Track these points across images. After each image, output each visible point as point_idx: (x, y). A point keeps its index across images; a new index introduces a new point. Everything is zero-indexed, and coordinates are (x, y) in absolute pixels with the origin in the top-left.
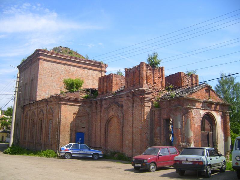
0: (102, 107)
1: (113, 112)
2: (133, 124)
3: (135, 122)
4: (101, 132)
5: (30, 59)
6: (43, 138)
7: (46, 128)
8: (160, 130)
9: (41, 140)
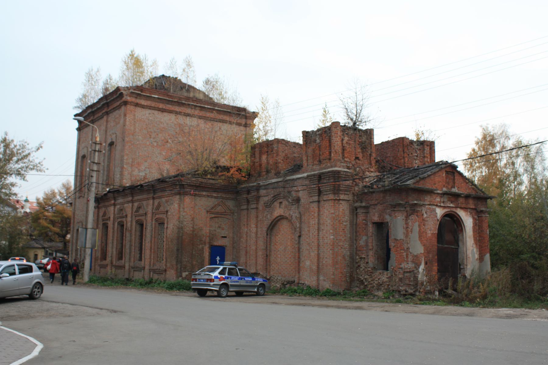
1: (281, 209)
3: (322, 227)
4: (258, 246)
5: (105, 102)
7: (153, 239)
8: (367, 241)
9: (140, 259)
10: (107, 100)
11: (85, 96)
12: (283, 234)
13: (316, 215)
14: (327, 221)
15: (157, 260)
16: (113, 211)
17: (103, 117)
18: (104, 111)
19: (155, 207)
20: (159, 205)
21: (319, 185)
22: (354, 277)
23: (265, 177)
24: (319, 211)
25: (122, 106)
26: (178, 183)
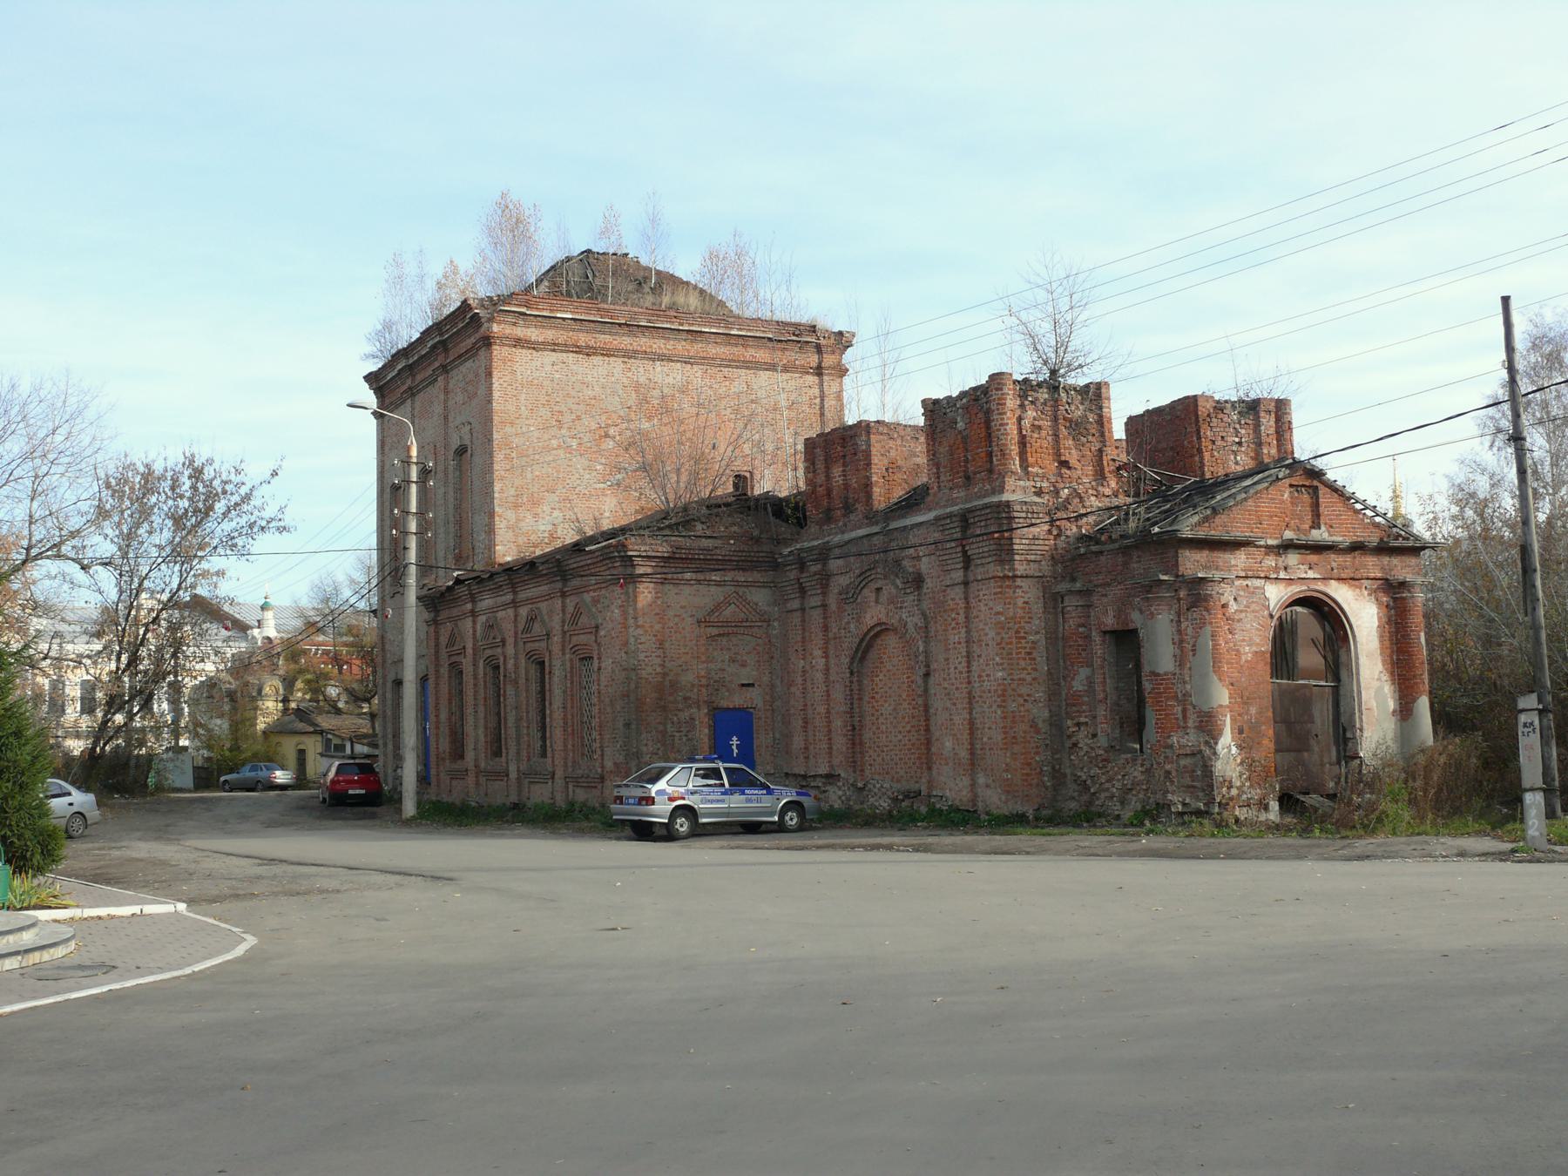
0: (827, 585)
2: (969, 662)
5: (438, 339)
6: (559, 746)
8: (1090, 681)
9: (544, 755)
10: (441, 335)
11: (388, 326)
12: (889, 671)
13: (961, 618)
14: (986, 634)
15: (583, 754)
16: (471, 631)
17: (436, 380)
18: (437, 364)
19: (521, 627)
20: (577, 615)
21: (964, 543)
22: (1065, 775)
23: (841, 524)
24: (968, 608)
25: (480, 348)
26: (616, 554)
